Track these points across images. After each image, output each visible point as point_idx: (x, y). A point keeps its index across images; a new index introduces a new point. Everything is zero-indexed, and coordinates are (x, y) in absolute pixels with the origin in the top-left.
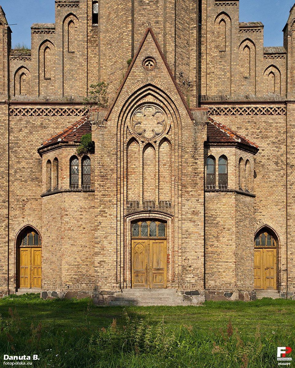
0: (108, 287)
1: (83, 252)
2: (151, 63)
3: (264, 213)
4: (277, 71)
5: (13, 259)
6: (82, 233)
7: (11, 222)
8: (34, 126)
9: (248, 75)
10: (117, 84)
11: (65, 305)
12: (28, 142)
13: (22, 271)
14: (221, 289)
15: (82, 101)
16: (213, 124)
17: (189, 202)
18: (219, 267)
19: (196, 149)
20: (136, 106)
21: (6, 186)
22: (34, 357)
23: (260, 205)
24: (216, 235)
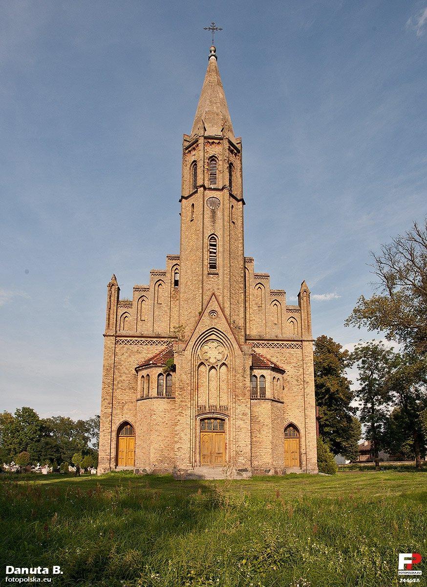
0: (184, 466)
2: (215, 314)
3: (290, 414)
8: (132, 352)
10: (192, 327)
11: (153, 479)
13: (120, 454)
15: (166, 336)
20: (204, 341)
22: (54, 570)
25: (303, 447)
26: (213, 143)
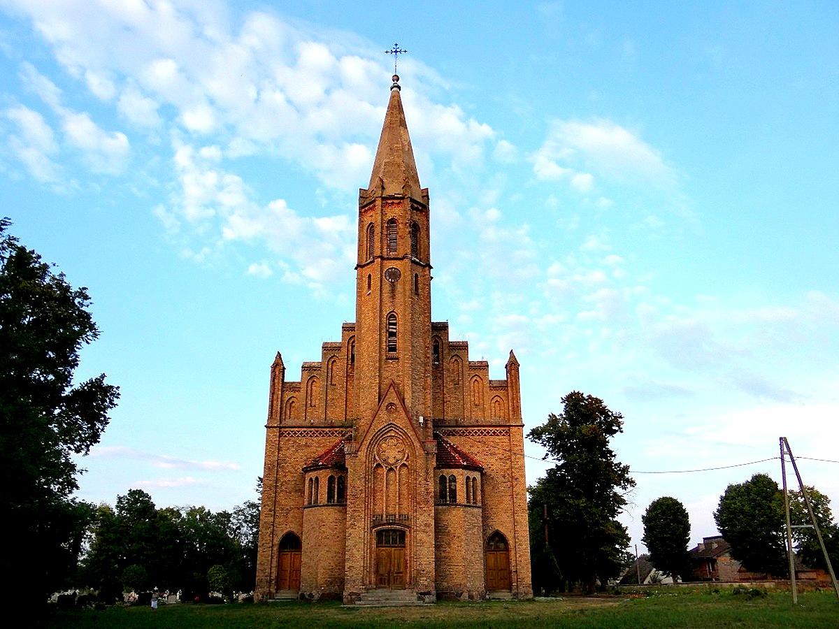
8: (299, 445)
25: (513, 563)
26: (393, 203)
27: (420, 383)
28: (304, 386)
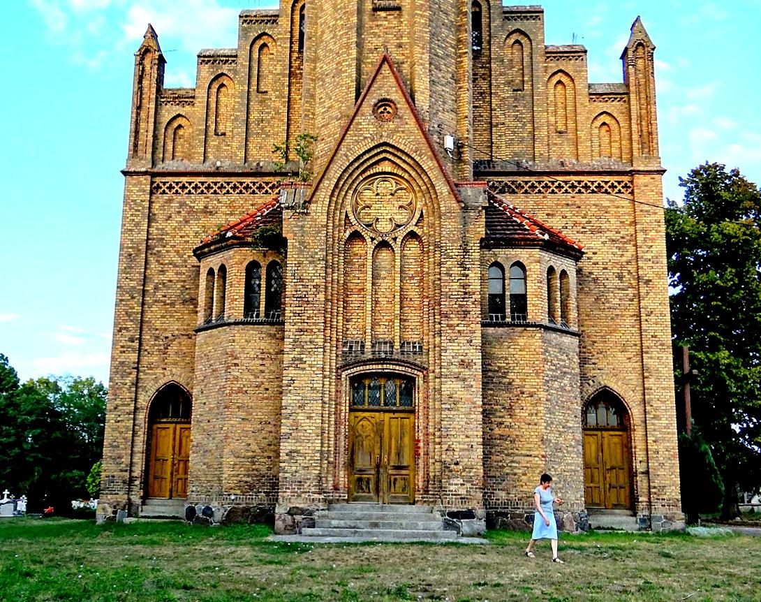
1: (264, 434)
2: (389, 109)
4: (614, 121)
5: (141, 444)
6: (263, 399)
7: (142, 377)
8: (191, 211)
9: (563, 129)
12: (181, 237)
14: (519, 508)
16: (501, 208)
17: (454, 344)
18: (514, 465)
19: (466, 251)
21: (138, 313)
23: (592, 350)
24: (507, 406)
25: (640, 455)
27: (447, 67)
28: (201, 95)
